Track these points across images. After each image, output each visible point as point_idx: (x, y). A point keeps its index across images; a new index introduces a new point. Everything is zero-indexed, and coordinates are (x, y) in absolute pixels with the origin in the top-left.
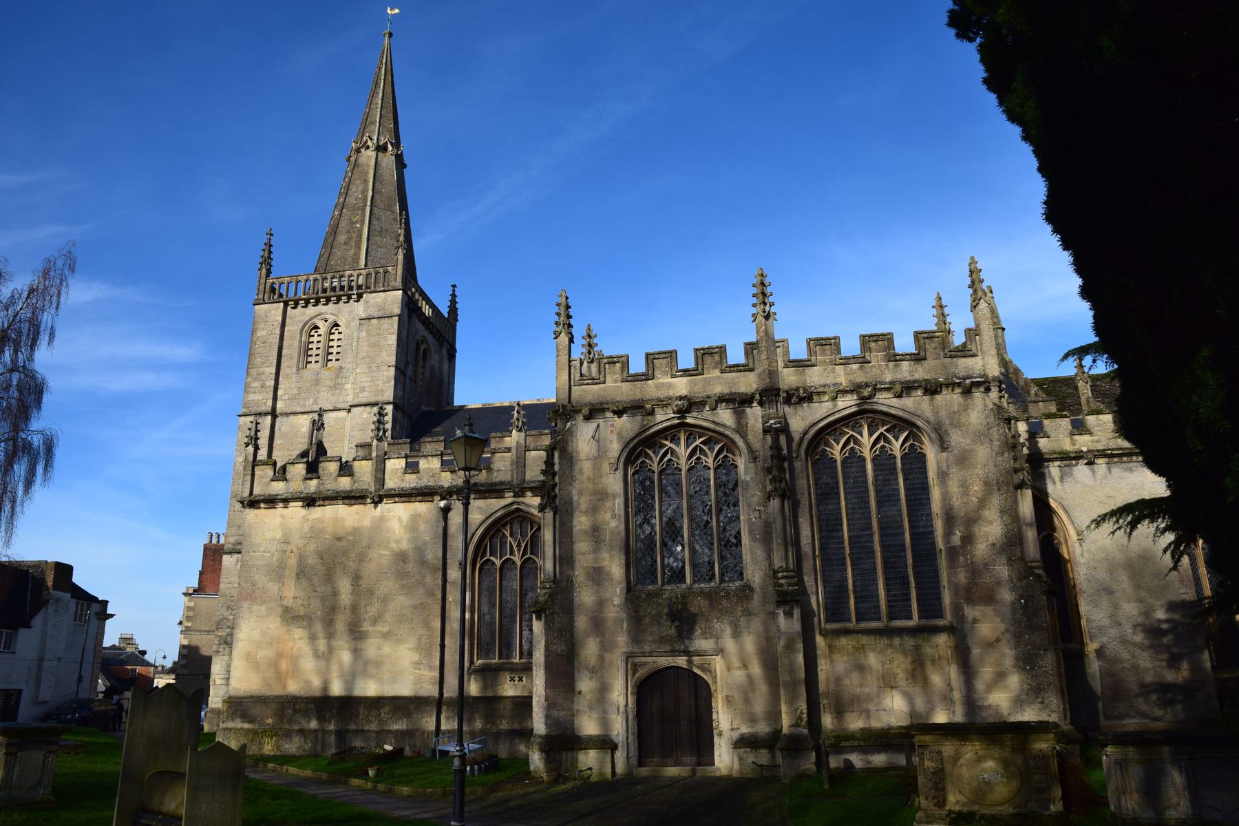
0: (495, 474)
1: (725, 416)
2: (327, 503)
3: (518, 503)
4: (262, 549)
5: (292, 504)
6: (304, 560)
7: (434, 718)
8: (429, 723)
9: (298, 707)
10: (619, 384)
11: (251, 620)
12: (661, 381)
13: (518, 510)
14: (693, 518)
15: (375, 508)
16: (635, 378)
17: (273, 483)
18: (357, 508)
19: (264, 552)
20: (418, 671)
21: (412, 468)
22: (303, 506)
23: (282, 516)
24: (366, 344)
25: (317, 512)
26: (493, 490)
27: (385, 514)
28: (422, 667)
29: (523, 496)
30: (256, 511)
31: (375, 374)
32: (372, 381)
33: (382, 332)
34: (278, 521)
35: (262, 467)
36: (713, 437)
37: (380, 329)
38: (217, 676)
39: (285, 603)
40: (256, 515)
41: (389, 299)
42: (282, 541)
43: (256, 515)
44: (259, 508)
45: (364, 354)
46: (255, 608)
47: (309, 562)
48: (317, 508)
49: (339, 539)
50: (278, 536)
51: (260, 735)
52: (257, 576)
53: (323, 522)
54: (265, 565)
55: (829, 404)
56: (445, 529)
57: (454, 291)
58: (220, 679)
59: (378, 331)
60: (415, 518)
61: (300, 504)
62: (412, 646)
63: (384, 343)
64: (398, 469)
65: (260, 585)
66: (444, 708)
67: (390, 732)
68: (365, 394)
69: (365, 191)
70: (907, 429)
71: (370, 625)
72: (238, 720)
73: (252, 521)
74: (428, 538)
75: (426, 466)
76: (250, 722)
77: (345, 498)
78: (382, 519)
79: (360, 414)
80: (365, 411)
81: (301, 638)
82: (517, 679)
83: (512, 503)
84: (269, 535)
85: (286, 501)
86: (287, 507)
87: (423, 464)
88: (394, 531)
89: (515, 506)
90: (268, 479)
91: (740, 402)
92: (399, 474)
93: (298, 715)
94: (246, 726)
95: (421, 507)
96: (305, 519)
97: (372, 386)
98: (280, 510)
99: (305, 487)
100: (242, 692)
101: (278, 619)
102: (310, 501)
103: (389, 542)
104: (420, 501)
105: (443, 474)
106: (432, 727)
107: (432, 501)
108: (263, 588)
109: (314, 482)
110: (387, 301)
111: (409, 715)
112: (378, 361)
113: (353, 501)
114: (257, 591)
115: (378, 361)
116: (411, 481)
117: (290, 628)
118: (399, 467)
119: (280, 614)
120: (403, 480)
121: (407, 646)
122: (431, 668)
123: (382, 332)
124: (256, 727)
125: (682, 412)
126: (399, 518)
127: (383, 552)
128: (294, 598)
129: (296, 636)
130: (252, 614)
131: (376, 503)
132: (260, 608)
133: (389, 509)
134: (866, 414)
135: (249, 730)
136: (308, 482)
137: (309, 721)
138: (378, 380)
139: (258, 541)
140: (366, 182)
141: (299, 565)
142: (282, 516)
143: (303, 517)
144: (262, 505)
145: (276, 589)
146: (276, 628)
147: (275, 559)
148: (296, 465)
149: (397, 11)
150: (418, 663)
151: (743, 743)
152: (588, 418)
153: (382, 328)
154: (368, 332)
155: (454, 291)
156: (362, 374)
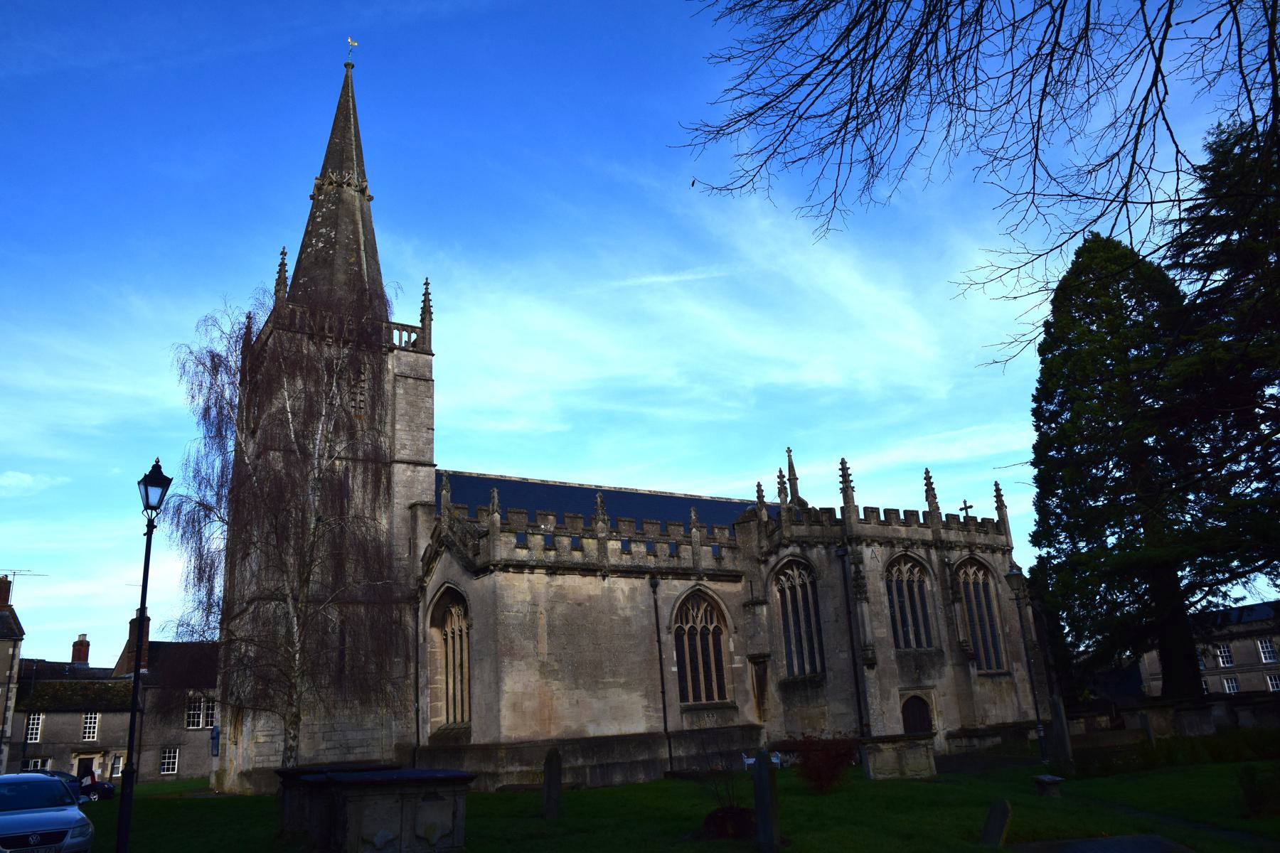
0: (683, 561)
1: (922, 552)
2: (566, 572)
4: (515, 610)
5: (537, 571)
6: (553, 621)
7: (667, 749)
8: (664, 753)
9: (566, 748)
10: (877, 526)
11: (513, 673)
12: (895, 527)
13: (699, 590)
14: (406, 578)
17: (517, 550)
18: (588, 579)
19: (517, 612)
21: (626, 549)
22: (546, 574)
23: (529, 580)
24: (404, 402)
25: (559, 580)
26: (682, 574)
27: (612, 586)
29: (702, 580)
30: (505, 574)
31: (415, 433)
32: (413, 440)
34: (526, 585)
36: (916, 563)
37: (417, 390)
38: (259, 733)
39: (540, 658)
40: (506, 578)
41: (420, 362)
43: (506, 578)
44: (509, 572)
45: (403, 412)
46: (516, 663)
48: (558, 576)
49: (579, 605)
50: (528, 598)
51: (539, 775)
53: (564, 588)
54: (520, 624)
55: (959, 552)
57: (427, 289)
58: (263, 736)
59: (415, 391)
62: (642, 693)
63: (422, 405)
64: (616, 549)
65: (517, 642)
66: (672, 740)
67: (637, 762)
68: (407, 452)
69: (356, 232)
70: (911, 562)
71: (611, 678)
72: (517, 764)
73: (503, 583)
74: (643, 608)
75: (636, 549)
76: (527, 765)
79: (404, 471)
80: (408, 468)
82: (711, 715)
83: (695, 586)
84: (520, 597)
85: (532, 569)
86: (533, 573)
88: (620, 600)
89: (698, 587)
90: (513, 546)
91: (927, 545)
92: (618, 554)
94: (525, 768)
99: (545, 556)
100: (513, 739)
101: (537, 673)
102: (554, 570)
103: (617, 609)
104: (636, 578)
105: (649, 557)
106: (668, 756)
107: (644, 578)
108: (520, 645)
109: (552, 553)
110: (418, 362)
114: (515, 648)
116: (626, 560)
117: (549, 680)
118: (617, 547)
120: (621, 559)
123: (419, 393)
124: (534, 769)
125: (906, 548)
126: (622, 590)
129: (554, 688)
130: (514, 669)
133: (613, 581)
134: (972, 561)
135: (528, 772)
136: (547, 552)
137: (577, 759)
139: (510, 602)
140: (354, 223)
142: (529, 580)
143: (548, 583)
144: (511, 569)
145: (532, 646)
150: (648, 707)
151: (950, 736)
153: (419, 389)
154: (405, 389)
155: (427, 289)
156: (402, 430)
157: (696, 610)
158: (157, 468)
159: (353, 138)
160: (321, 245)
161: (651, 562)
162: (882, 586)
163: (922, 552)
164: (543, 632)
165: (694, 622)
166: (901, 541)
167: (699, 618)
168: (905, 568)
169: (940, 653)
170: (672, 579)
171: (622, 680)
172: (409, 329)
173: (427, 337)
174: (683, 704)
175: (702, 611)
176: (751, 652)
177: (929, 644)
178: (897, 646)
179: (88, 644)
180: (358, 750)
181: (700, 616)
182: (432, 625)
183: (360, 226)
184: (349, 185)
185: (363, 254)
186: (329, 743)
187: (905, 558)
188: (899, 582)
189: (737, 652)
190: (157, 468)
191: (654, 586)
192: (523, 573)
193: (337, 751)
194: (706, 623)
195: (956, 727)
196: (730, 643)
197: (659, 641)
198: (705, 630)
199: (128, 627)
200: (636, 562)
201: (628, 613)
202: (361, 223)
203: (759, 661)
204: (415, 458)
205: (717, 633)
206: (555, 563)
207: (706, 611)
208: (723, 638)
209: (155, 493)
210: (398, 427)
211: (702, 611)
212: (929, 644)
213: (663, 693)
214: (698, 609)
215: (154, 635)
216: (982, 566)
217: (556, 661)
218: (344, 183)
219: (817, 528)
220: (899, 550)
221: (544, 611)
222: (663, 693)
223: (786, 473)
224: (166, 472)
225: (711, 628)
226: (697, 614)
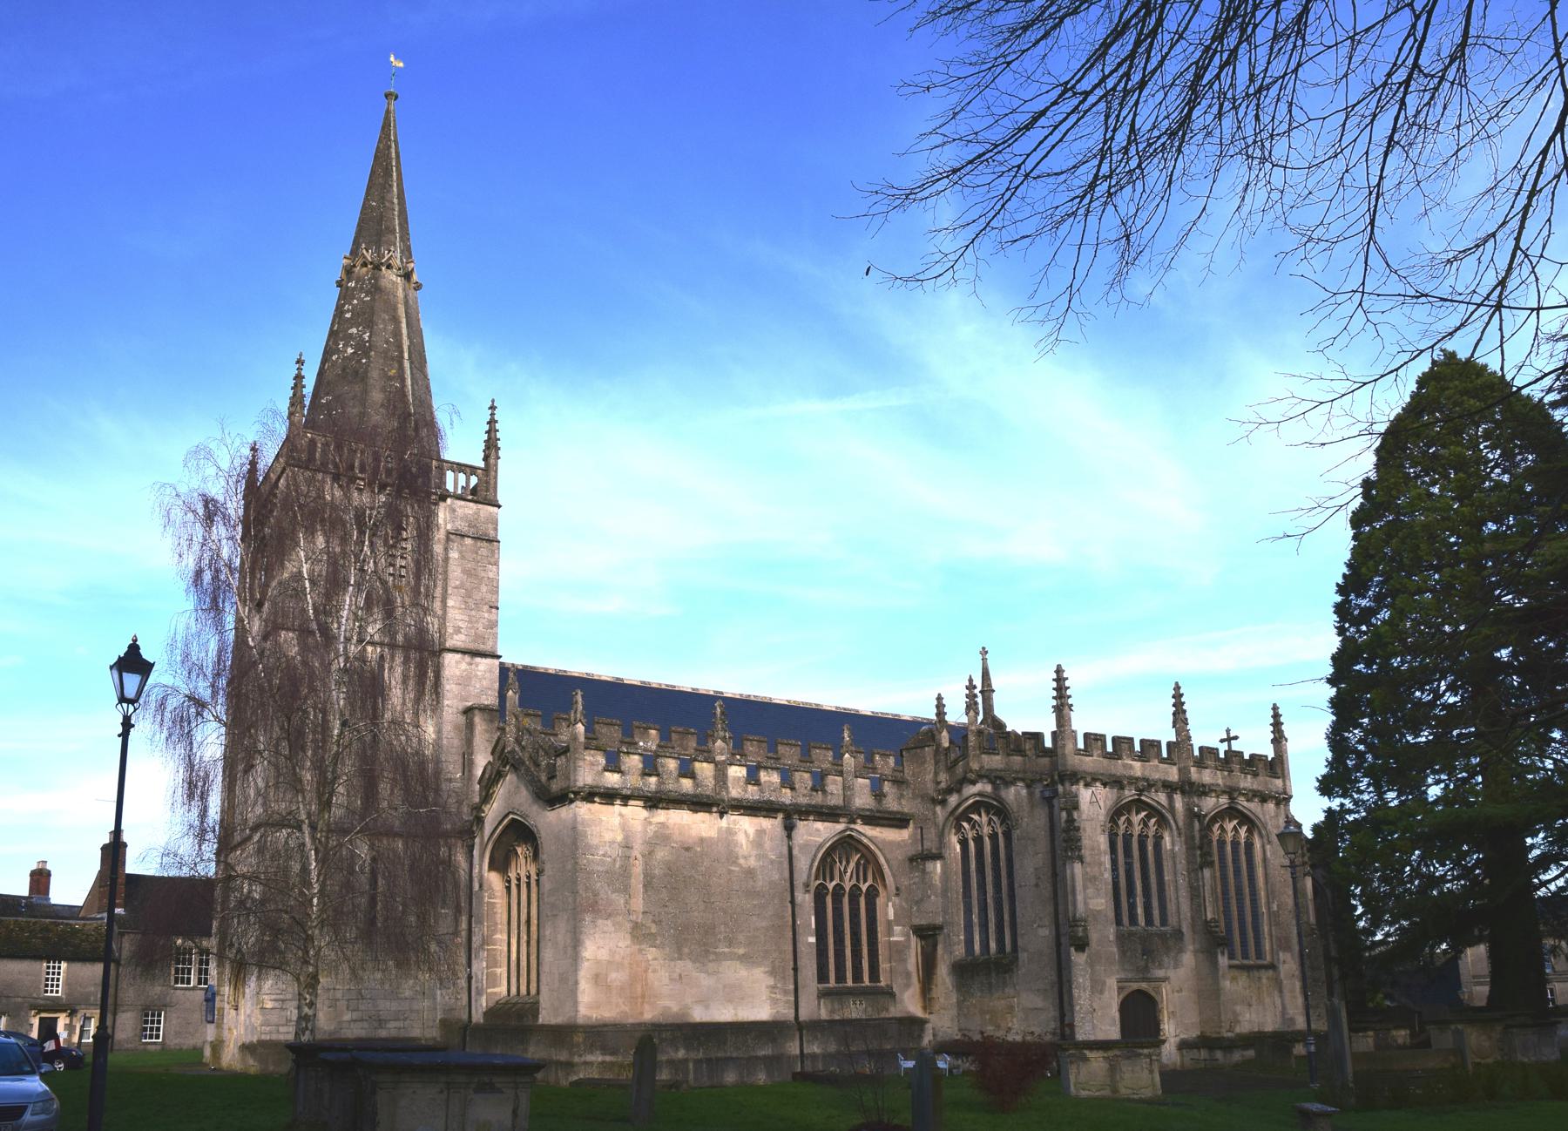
0: (829, 797)
1: (1162, 798)
3: (852, 830)
4: (601, 853)
5: (631, 802)
7: (797, 1043)
15: (721, 817)
16: (1107, 756)
17: (607, 774)
18: (701, 816)
19: (604, 855)
20: (774, 996)
21: (752, 778)
23: (621, 815)
25: (661, 816)
28: (777, 991)
29: (855, 823)
31: (473, 613)
33: (479, 557)
34: (616, 821)
35: (592, 752)
36: (1153, 811)
37: (477, 553)
39: (633, 918)
42: (623, 845)
44: (594, 802)
47: (656, 872)
48: (660, 811)
49: (687, 849)
50: (619, 838)
52: (599, 884)
54: (607, 872)
55: (1214, 800)
56: (790, 849)
60: (761, 832)
61: (640, 803)
63: (483, 574)
64: (739, 778)
65: (602, 895)
66: (804, 1032)
67: (757, 1058)
69: (397, 334)
74: (773, 857)
75: (767, 778)
76: (612, 1054)
77: (694, 803)
78: (730, 832)
81: (655, 959)
84: (608, 837)
85: (625, 800)
87: (764, 776)
89: (848, 833)
90: (600, 768)
91: (1169, 787)
93: (664, 1044)
94: (608, 1058)
95: (766, 823)
96: (647, 822)
97: (471, 628)
98: (617, 808)
101: (628, 936)
102: (654, 802)
103: (737, 858)
105: (784, 790)
109: (653, 780)
111: (774, 1040)
112: (477, 596)
113: (698, 808)
114: (600, 902)
115: (477, 596)
116: (752, 793)
117: (643, 947)
119: (630, 930)
120: (746, 791)
121: (762, 969)
122: (786, 992)
125: (1141, 791)
127: (733, 868)
128: (643, 913)
131: (722, 814)
132: (606, 922)
133: (735, 821)
134: (1232, 812)
135: (612, 1063)
137: (677, 1050)
138: (477, 622)
140: (396, 320)
141: (646, 875)
142: (621, 815)
143: (645, 819)
144: (597, 799)
145: (622, 901)
146: (627, 947)
147: (617, 866)
148: (631, 756)
149: (401, 65)
151: (1183, 1045)
152: (1087, 785)
157: (844, 863)
158: (134, 648)
159: (396, 201)
160: (350, 351)
161: (786, 796)
162: (1103, 841)
163: (1162, 798)
164: (637, 883)
165: (841, 879)
166: (1133, 780)
167: (849, 874)
168: (1137, 819)
169: (1178, 934)
170: (814, 820)
171: (741, 951)
172: (468, 470)
173: (492, 482)
174: (821, 986)
175: (852, 865)
176: (917, 921)
177: (1164, 922)
178: (1119, 922)
179: (49, 874)
180: (392, 1025)
181: (849, 871)
182: (492, 867)
183: (404, 325)
184: (389, 267)
185: (407, 364)
186: (355, 1013)
187: (1139, 805)
188: (1128, 838)
189: (897, 921)
190: (134, 648)
191: (789, 828)
192: (613, 804)
193: (366, 1025)
194: (858, 880)
195: (1193, 1034)
196: (888, 909)
197: (793, 902)
198: (855, 892)
199: (27, 880)
200: (766, 796)
201: (752, 862)
202: (404, 321)
203: (928, 935)
204: (472, 646)
205: (872, 894)
206: (656, 792)
207: (858, 864)
208: (880, 901)
209: (132, 681)
210: (450, 603)
211: (852, 865)
212: (1164, 922)
213: (795, 969)
214: (848, 863)
215: (134, 865)
216: (1245, 819)
217: (654, 921)
218: (382, 264)
219: (1017, 759)
220: (1130, 793)
221: (639, 856)
222: (795, 969)
223: (978, 682)
224: (147, 654)
225: (864, 888)
226: (845, 869)
